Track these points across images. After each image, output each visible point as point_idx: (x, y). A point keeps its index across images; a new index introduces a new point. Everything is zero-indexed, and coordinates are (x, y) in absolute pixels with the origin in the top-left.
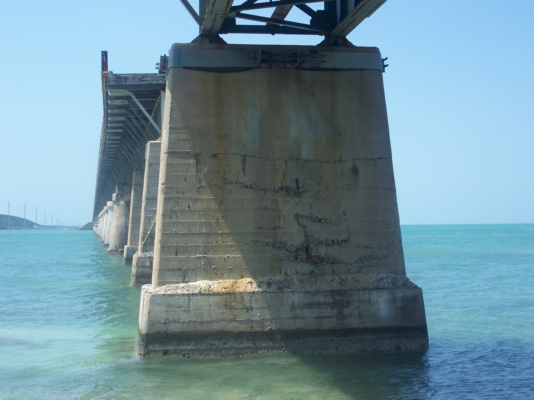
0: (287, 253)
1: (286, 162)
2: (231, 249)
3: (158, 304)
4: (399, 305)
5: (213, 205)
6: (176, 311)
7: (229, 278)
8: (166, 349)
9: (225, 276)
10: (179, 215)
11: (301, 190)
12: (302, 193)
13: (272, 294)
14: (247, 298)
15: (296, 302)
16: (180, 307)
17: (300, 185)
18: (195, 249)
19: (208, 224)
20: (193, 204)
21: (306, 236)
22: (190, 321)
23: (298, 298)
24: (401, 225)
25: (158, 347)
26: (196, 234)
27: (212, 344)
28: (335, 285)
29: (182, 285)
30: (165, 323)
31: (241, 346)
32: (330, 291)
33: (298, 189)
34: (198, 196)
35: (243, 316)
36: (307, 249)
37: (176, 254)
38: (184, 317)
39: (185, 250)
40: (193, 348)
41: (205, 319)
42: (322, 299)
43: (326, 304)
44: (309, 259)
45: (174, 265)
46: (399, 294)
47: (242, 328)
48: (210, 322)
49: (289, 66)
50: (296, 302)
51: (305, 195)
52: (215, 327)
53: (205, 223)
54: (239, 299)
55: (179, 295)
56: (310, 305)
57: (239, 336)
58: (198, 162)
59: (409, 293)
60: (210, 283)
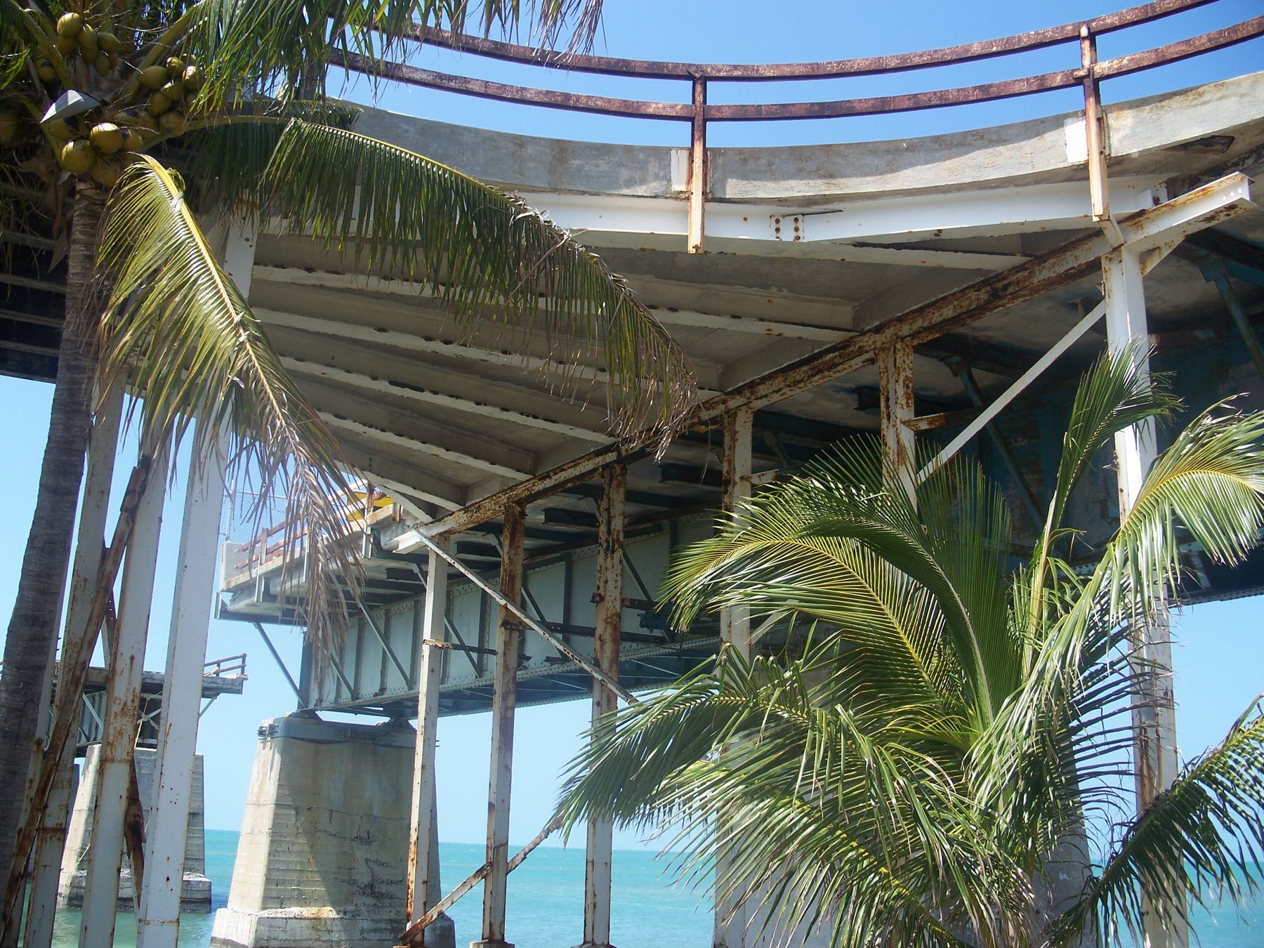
4: (438, 932)
5: (306, 848)
7: (315, 906)
11: (371, 839)
12: (371, 842)
14: (329, 922)
15: (365, 927)
16: (279, 927)
18: (291, 882)
19: (302, 863)
22: (286, 940)
23: (366, 925)
24: (210, 831)
28: (393, 916)
29: (280, 910)
32: (390, 920)
34: (295, 840)
36: (372, 886)
38: (282, 936)
39: (284, 882)
41: (297, 938)
43: (386, 929)
44: (373, 894)
45: (274, 894)
49: (368, 742)
50: (365, 927)
51: (374, 844)
53: (299, 862)
54: (323, 923)
56: (375, 931)
59: (446, 923)
60: (301, 909)
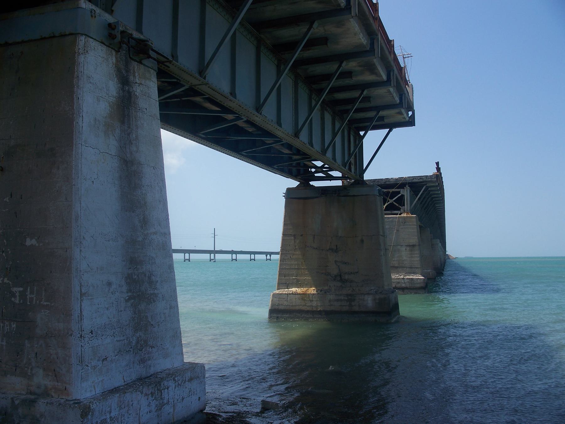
0: (331, 277)
1: (332, 237)
2: (308, 275)
3: (275, 297)
6: (282, 301)
8: (278, 316)
9: (304, 286)
10: (286, 260)
13: (321, 295)
14: (311, 296)
17: (338, 248)
20: (292, 256)
21: (339, 270)
22: (288, 305)
25: (275, 315)
26: (293, 269)
27: (296, 315)
30: (278, 305)
31: (308, 316)
32: (346, 294)
33: (337, 249)
35: (309, 304)
36: (340, 276)
37: (285, 277)
38: (286, 303)
40: (288, 316)
42: (343, 298)
46: (378, 297)
47: (308, 309)
48: (295, 306)
52: (297, 308)
55: (284, 294)
56: (338, 300)
57: (307, 312)
58: (295, 238)
60: (297, 289)
